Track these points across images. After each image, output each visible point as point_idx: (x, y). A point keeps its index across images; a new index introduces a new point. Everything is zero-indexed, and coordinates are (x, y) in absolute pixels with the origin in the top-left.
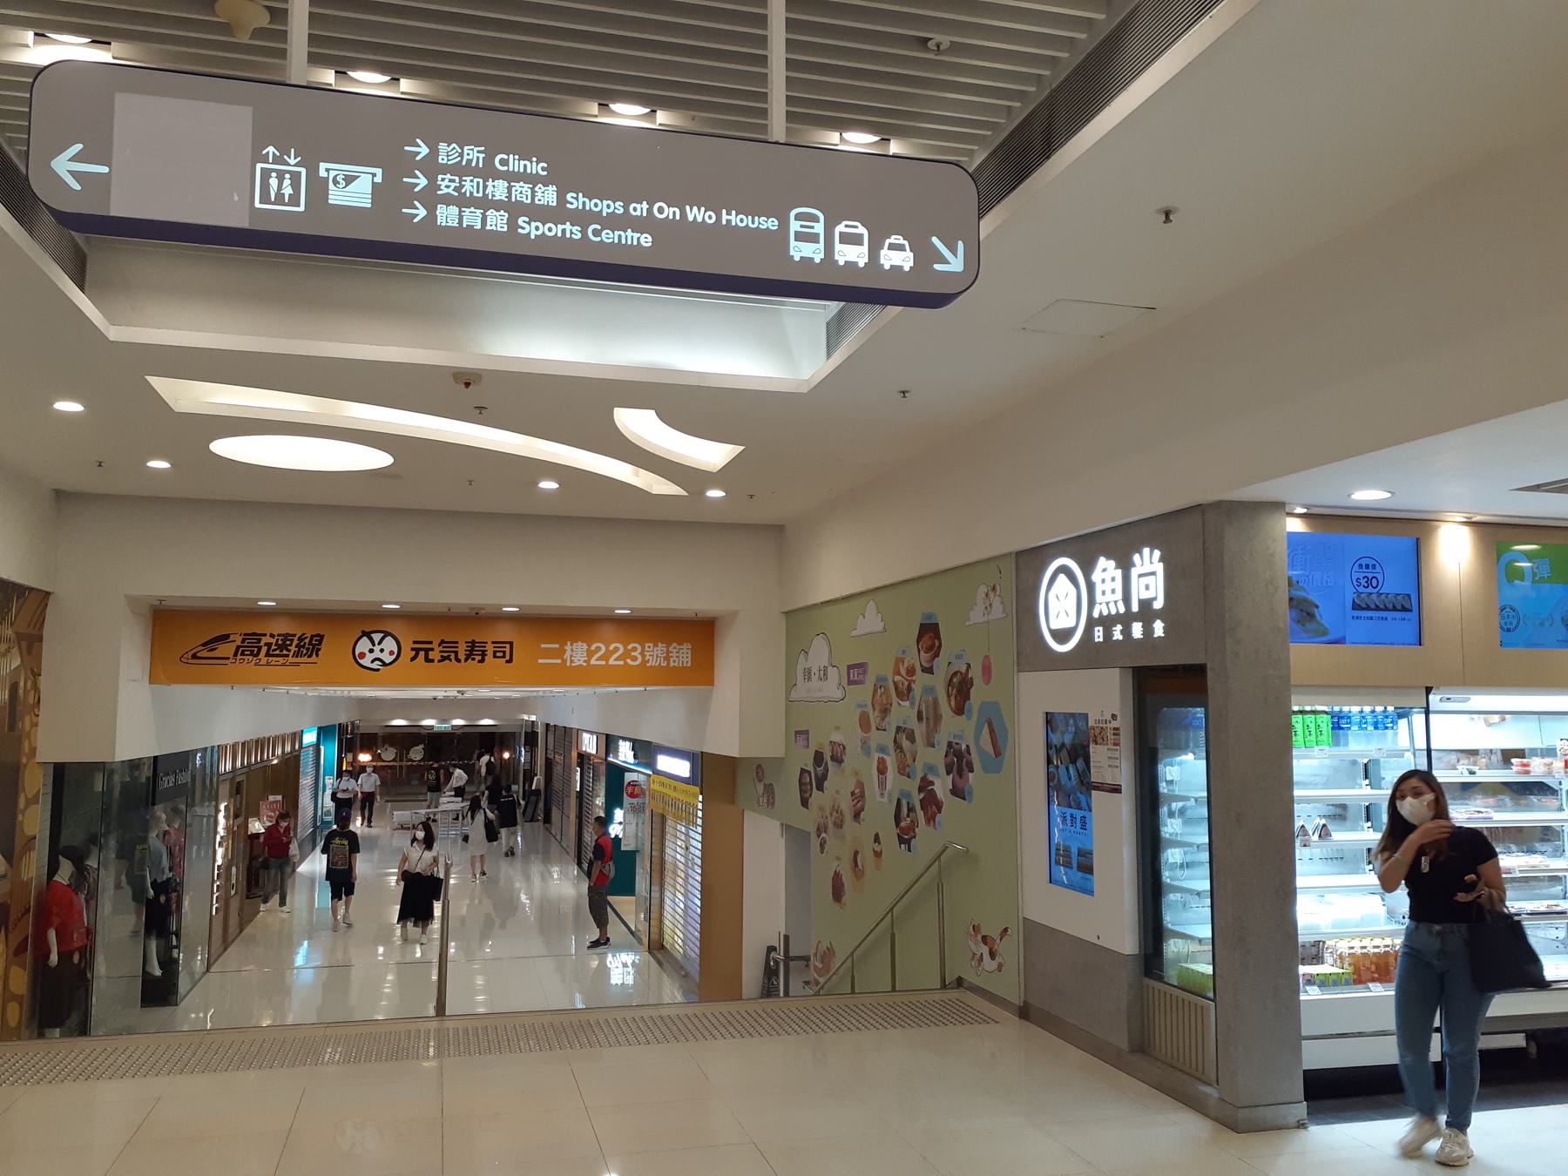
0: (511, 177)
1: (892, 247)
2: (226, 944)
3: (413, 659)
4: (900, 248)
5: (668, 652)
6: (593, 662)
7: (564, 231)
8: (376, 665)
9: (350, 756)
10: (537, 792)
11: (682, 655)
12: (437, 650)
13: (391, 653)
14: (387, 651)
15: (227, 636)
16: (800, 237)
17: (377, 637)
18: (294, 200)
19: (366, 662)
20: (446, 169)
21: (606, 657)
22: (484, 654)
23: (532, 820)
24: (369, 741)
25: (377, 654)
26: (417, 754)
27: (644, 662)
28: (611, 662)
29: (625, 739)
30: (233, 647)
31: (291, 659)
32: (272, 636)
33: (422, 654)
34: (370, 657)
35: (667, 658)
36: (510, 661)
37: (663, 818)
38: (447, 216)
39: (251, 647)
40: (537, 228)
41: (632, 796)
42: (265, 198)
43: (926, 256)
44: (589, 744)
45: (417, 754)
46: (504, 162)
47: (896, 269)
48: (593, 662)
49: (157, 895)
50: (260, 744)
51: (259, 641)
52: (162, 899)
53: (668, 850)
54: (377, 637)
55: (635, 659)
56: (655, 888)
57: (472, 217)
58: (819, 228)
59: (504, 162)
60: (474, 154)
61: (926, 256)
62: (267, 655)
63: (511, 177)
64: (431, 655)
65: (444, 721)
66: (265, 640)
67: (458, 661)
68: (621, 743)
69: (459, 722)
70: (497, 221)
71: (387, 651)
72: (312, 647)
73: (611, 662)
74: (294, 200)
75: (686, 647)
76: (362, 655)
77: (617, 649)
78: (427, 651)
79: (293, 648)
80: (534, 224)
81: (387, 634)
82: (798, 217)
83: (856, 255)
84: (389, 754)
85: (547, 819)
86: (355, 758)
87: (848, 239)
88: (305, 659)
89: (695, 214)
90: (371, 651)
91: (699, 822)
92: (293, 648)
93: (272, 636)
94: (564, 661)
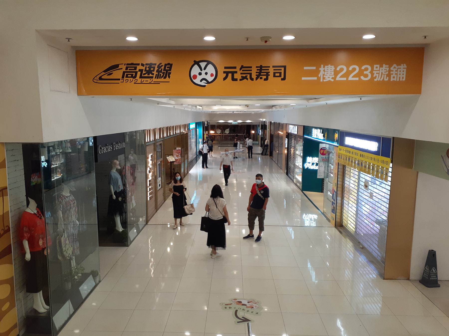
2: (157, 209)
3: (225, 79)
5: (390, 71)
6: (338, 78)
8: (203, 83)
9: (207, 132)
10: (267, 145)
11: (399, 73)
12: (239, 72)
13: (212, 75)
14: (209, 74)
15: (117, 66)
17: (203, 65)
19: (197, 81)
21: (347, 75)
22: (267, 75)
23: (265, 155)
24: (213, 127)
25: (203, 76)
26: (227, 131)
27: (373, 78)
28: (350, 78)
29: (316, 128)
30: (121, 72)
31: (154, 80)
32: (143, 65)
33: (230, 75)
34: (199, 78)
35: (389, 75)
36: (284, 79)
37: (344, 167)
39: (131, 72)
41: (323, 154)
44: (293, 130)
45: (227, 131)
48: (338, 78)
49: (117, 198)
50: (168, 129)
51: (136, 68)
52: (120, 199)
53: (346, 182)
54: (203, 65)
55: (366, 76)
56: (339, 199)
62: (141, 77)
64: (236, 76)
65: (235, 121)
66: (139, 67)
67: (252, 79)
68: (313, 130)
69: (240, 121)
71: (209, 74)
72: (165, 72)
73: (350, 78)
75: (403, 67)
76: (195, 77)
77: (354, 69)
78: (233, 73)
79: (155, 73)
81: (209, 63)
84: (219, 132)
85: (271, 155)
86: (209, 133)
88: (162, 80)
90: (200, 74)
91: (389, 179)
92: (155, 73)
93: (143, 65)
94: (319, 78)
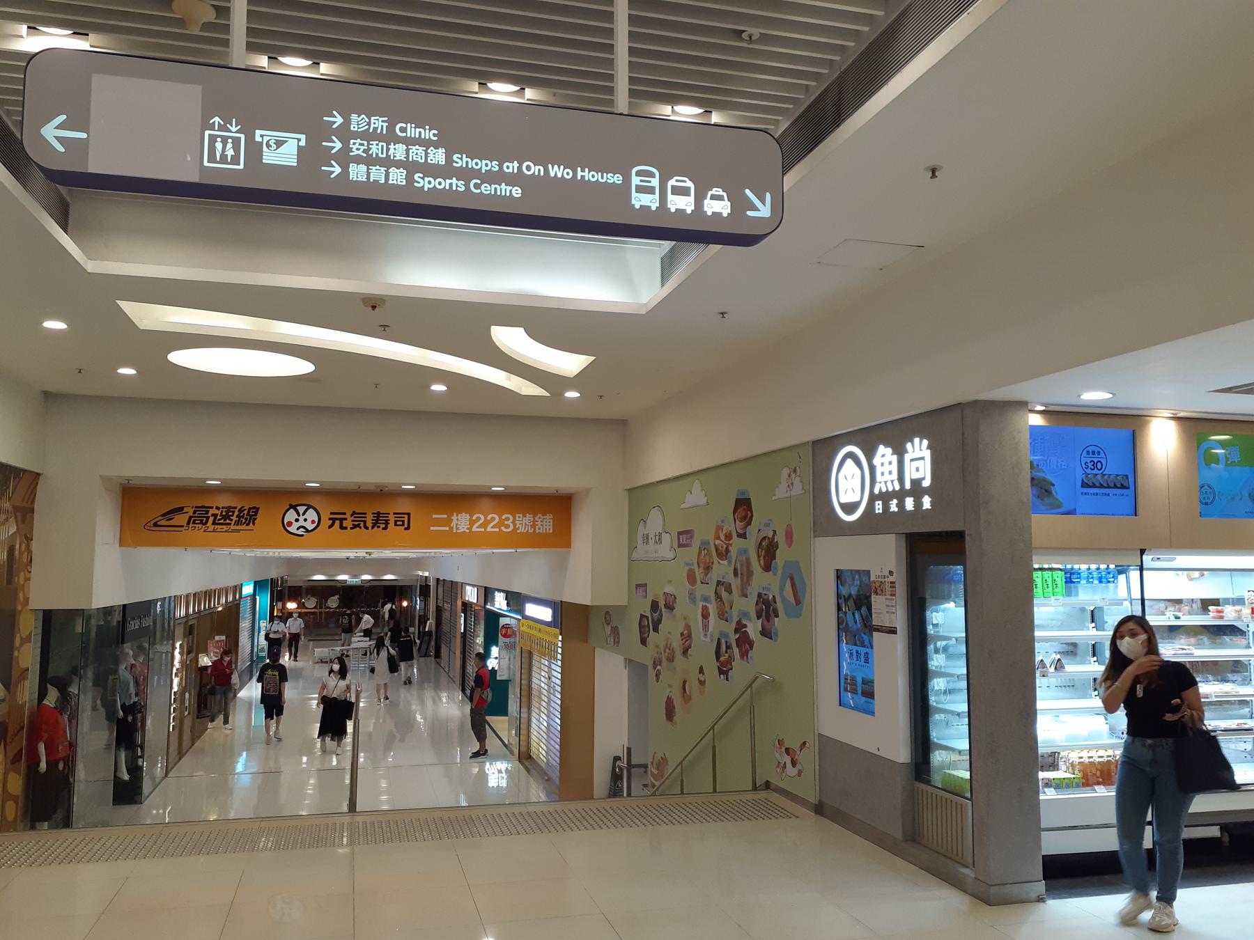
0: (409, 142)
1: (714, 197)
2: (181, 755)
3: (330, 527)
4: (720, 198)
5: (534, 521)
6: (474, 529)
7: (451, 185)
8: (300, 532)
9: (280, 604)
10: (430, 633)
11: (546, 524)
12: (350, 519)
13: (313, 522)
14: (309, 521)
15: (182, 509)
16: (640, 189)
17: (301, 509)
18: (235, 160)
19: (293, 529)
20: (356, 135)
21: (484, 525)
22: (387, 523)
23: (425, 656)
24: (295, 593)
25: (301, 523)
26: (333, 602)
27: (515, 529)
28: (489, 529)
29: (500, 591)
30: (186, 517)
31: (232, 527)
32: (218, 508)
33: (337, 523)
34: (296, 525)
35: (533, 526)
36: (408, 528)
37: (530, 654)
38: (357, 172)
39: (200, 517)
40: (430, 183)
41: (506, 636)
42: (212, 158)
43: (740, 205)
44: (471, 595)
45: (333, 602)
46: (403, 130)
47: (717, 215)
48: (474, 529)
49: (126, 715)
50: (208, 594)
51: (207, 512)
52: (130, 718)
53: (534, 680)
54: (301, 509)
55: (508, 526)
56: (524, 710)
57: (378, 174)
58: (655, 182)
59: (403, 130)
60: (379, 123)
61: (740, 205)
62: (214, 523)
63: (409, 142)
64: (345, 524)
65: (355, 576)
66: (212, 511)
67: (367, 528)
68: (497, 594)
69: (367, 577)
70: (398, 177)
71: (309, 521)
72: (249, 517)
73: (489, 529)
74: (235, 160)
75: (549, 517)
76: (290, 524)
77: (493, 519)
78: (341, 520)
79: (234, 518)
80: (427, 179)
81: (309, 507)
82: (638, 174)
83: (685, 204)
84: (311, 603)
85: (438, 655)
86: (284, 606)
87: (678, 191)
88: (244, 527)
89: (556, 171)
90: (297, 520)
91: (559, 657)
92: (234, 518)
93: (218, 508)
94: (451, 528)
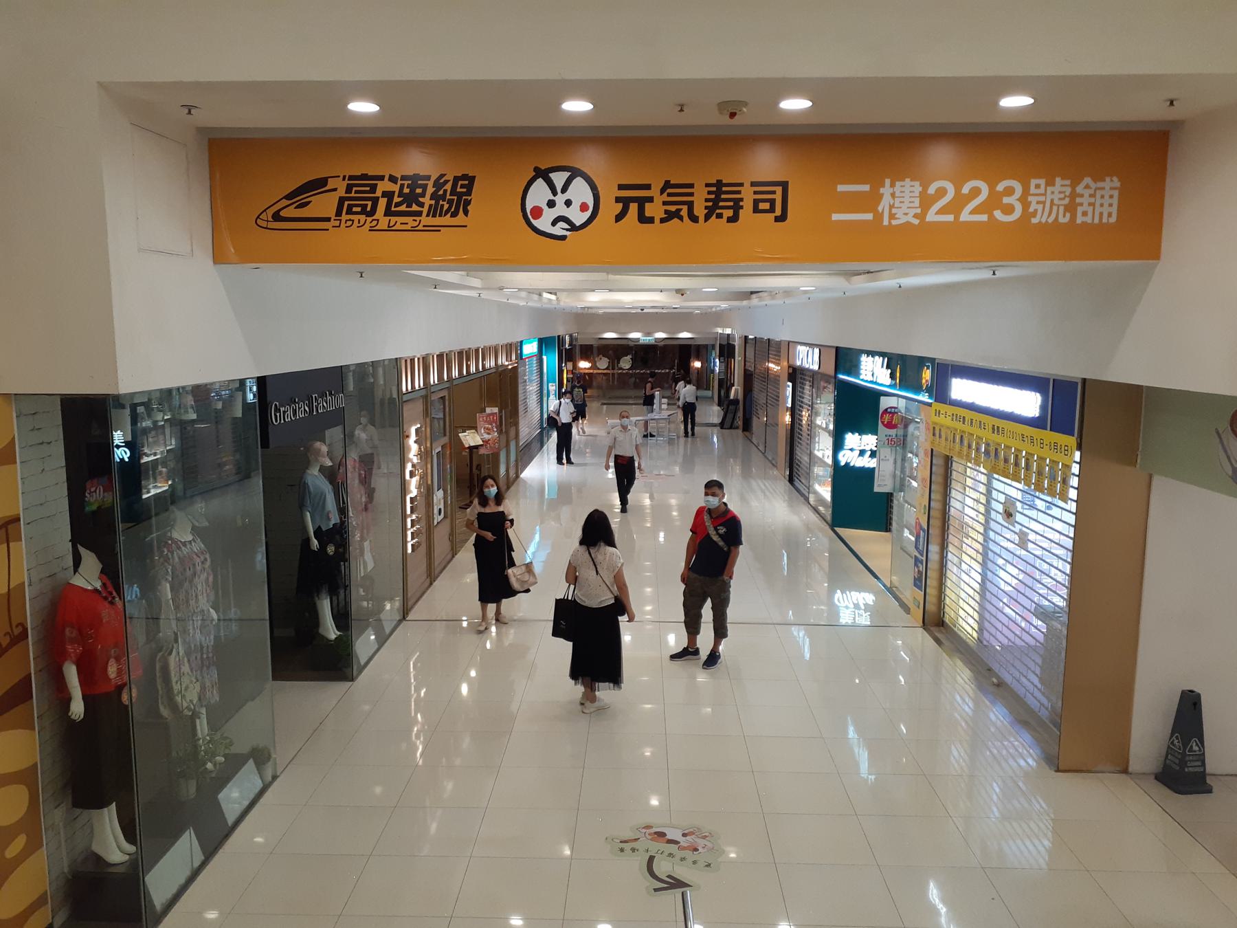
2: (432, 577)
3: (619, 218)
5: (1073, 195)
6: (931, 216)
8: (559, 230)
9: (570, 365)
10: (736, 402)
11: (1101, 201)
12: (659, 199)
13: (584, 207)
14: (576, 205)
15: (322, 182)
17: (559, 178)
19: (543, 224)
21: (955, 206)
22: (737, 206)
23: (731, 428)
24: (587, 352)
25: (560, 210)
26: (626, 363)
27: (1027, 215)
28: (965, 216)
29: (872, 353)
30: (333, 199)
31: (426, 220)
32: (393, 179)
33: (634, 207)
34: (549, 215)
35: (1071, 208)
36: (782, 218)
37: (948, 460)
39: (360, 199)
41: (890, 425)
44: (808, 359)
45: (626, 363)
48: (931, 216)
49: (323, 546)
50: (464, 355)
51: (373, 189)
52: (331, 550)
53: (953, 503)
54: (559, 178)
55: (1009, 210)
56: (934, 548)
62: (388, 213)
64: (650, 210)
65: (648, 334)
66: (383, 186)
67: (694, 219)
68: (864, 358)
69: (661, 335)
71: (576, 205)
72: (456, 198)
73: (965, 216)
75: (1111, 185)
76: (537, 212)
77: (976, 192)
78: (641, 202)
79: (427, 200)
81: (575, 173)
84: (603, 363)
85: (747, 427)
86: (575, 366)
88: (447, 220)
90: (551, 204)
91: (1073, 494)
92: (427, 200)
93: (393, 179)
94: (879, 217)
